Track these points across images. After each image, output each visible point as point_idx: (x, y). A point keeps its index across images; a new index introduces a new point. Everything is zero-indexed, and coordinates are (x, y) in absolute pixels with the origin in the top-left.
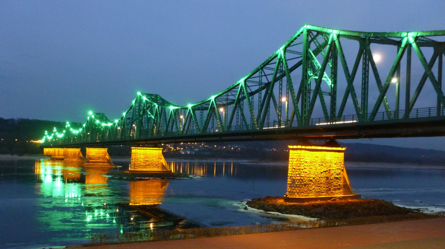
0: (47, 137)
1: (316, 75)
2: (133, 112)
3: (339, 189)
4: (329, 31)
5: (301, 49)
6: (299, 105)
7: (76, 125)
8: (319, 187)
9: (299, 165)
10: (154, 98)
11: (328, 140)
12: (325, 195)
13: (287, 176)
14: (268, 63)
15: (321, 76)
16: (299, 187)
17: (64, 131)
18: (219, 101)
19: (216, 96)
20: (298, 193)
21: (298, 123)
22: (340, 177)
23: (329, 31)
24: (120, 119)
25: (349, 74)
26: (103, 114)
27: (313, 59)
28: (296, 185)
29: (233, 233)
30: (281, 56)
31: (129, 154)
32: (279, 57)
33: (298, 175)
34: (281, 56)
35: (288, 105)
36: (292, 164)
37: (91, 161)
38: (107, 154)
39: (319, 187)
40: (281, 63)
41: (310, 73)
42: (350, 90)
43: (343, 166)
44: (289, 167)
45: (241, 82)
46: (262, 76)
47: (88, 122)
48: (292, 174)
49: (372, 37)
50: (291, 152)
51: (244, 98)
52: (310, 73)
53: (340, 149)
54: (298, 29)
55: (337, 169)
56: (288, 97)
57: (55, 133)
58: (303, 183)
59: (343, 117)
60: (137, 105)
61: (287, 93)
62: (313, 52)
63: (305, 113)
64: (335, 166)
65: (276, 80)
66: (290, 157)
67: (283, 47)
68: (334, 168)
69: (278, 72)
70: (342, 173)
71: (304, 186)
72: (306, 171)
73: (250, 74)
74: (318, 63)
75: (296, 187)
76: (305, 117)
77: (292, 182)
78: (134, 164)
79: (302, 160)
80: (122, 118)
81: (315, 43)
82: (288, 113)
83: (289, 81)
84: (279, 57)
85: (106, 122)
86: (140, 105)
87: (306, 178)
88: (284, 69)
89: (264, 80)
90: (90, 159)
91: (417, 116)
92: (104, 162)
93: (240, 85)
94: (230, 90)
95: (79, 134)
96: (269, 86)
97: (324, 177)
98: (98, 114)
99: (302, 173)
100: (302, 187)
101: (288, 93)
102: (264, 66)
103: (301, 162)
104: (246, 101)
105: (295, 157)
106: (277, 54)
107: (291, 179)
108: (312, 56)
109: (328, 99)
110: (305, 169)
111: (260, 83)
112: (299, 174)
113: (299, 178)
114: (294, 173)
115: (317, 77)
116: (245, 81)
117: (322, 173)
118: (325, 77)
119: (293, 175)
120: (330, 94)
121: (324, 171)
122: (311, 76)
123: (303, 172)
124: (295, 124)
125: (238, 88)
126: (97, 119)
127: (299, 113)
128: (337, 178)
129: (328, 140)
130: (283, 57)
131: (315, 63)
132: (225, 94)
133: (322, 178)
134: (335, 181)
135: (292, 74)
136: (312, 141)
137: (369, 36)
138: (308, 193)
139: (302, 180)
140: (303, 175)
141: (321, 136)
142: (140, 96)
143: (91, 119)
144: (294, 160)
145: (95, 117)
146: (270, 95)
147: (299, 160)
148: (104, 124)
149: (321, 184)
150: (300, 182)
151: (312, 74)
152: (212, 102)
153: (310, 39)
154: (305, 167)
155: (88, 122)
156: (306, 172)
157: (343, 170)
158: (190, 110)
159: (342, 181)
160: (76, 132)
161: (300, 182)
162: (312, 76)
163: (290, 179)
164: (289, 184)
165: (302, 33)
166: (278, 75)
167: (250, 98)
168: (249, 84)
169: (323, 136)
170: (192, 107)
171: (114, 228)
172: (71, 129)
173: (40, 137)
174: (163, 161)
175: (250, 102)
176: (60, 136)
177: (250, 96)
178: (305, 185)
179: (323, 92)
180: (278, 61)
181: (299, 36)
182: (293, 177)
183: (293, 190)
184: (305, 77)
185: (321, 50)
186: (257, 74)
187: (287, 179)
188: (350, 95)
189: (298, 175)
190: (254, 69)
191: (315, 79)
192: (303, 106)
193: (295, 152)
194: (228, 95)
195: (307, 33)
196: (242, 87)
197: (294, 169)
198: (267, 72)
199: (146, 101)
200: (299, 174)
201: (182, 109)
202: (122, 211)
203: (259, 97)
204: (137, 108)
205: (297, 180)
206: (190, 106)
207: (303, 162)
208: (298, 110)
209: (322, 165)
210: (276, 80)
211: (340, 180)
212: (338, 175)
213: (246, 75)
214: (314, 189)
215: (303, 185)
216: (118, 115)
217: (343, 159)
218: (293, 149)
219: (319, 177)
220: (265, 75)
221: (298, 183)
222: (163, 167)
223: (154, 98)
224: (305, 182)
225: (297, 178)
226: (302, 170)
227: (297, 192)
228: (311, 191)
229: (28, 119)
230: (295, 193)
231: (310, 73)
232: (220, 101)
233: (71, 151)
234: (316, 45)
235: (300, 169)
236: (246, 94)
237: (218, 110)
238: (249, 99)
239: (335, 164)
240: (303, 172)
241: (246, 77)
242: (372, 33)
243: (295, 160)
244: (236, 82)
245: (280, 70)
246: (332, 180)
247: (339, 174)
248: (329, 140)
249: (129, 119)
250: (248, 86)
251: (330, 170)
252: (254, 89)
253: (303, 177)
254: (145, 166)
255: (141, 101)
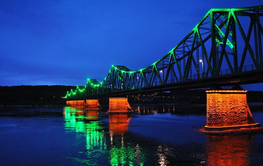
0: (68, 95)
1: (221, 41)
2: (110, 77)
3: (244, 120)
4: (228, 10)
5: (209, 26)
6: (212, 63)
7: (81, 87)
8: (230, 119)
9: (214, 104)
10: (120, 67)
11: (234, 86)
12: (235, 125)
13: (206, 112)
14: (187, 37)
15: (225, 42)
16: (215, 120)
17: (76, 91)
18: (159, 66)
19: (157, 62)
20: (215, 124)
21: (211, 74)
22: (245, 112)
23: (228, 10)
24: (103, 82)
25: (246, 37)
26: (95, 80)
27: (219, 31)
28: (213, 118)
29: (146, 112)
30: (196, 32)
31: (108, 102)
32: (195, 32)
33: (214, 111)
34: (196, 32)
35: (204, 64)
36: (209, 103)
37: (89, 107)
38: (98, 103)
39: (230, 119)
40: (197, 37)
41: (217, 40)
42: (248, 47)
43: (246, 103)
44: (207, 106)
45: (172, 52)
46: (184, 47)
47: (87, 84)
48: (209, 111)
49: (260, 9)
50: (208, 95)
51: (174, 63)
52: (217, 40)
53: (243, 91)
54: (206, 12)
55: (243, 106)
56: (203, 59)
57: (72, 93)
58: (218, 117)
59: (244, 67)
60: (112, 72)
61: (203, 57)
62: (219, 27)
63: (216, 68)
64: (240, 104)
65: (193, 49)
66: (208, 98)
67: (197, 25)
68: (240, 106)
69: (195, 43)
70: (246, 109)
71: (219, 119)
72: (220, 108)
73: (177, 46)
74: (222, 34)
75: (213, 120)
76: (216, 70)
77: (210, 116)
78: (111, 108)
79: (216, 100)
80: (104, 81)
81: (219, 20)
82: (204, 69)
83: (204, 48)
84: (195, 32)
85: (94, 84)
86: (113, 73)
87: (220, 113)
88: (199, 41)
89: (187, 49)
90: (89, 106)
91: (245, 70)
92: (96, 108)
93: (171, 54)
94: (165, 58)
95: (83, 92)
96: (190, 53)
97: (233, 112)
98: (92, 80)
99: (217, 110)
100: (218, 120)
101: (203, 56)
102: (185, 40)
103: (216, 101)
104: (175, 65)
105: (211, 98)
106: (193, 30)
107: (209, 114)
108: (217, 29)
109: (231, 58)
110: (219, 106)
111: (184, 52)
112: (215, 110)
113: (215, 113)
114: (211, 110)
115: (222, 43)
116: (174, 51)
117: (231, 109)
118: (228, 43)
119: (210, 111)
120: (232, 54)
121: (233, 108)
122: (218, 42)
123: (218, 109)
124: (210, 75)
125: (170, 56)
126: (92, 83)
127: (211, 68)
128: (243, 113)
129: (234, 86)
130: (198, 32)
131: (220, 34)
132: (162, 61)
133: (232, 112)
134: (241, 115)
135: (205, 44)
136: (223, 87)
137: (258, 8)
138: (222, 124)
139: (217, 115)
140: (218, 111)
141: (228, 83)
142: (114, 67)
143: (89, 83)
144: (210, 100)
145: (91, 82)
146: (191, 58)
147: (214, 100)
148: (95, 86)
149: (231, 117)
150: (215, 116)
151: (218, 41)
152: (172, 55)
153: (215, 18)
154: (219, 105)
155: (87, 84)
156: (220, 109)
157: (246, 107)
158: (141, 73)
159: (247, 114)
160: (81, 91)
161: (215, 116)
162: (219, 42)
163: (208, 114)
164: (208, 118)
165: (209, 14)
166: (195, 46)
167: (179, 62)
168: (177, 53)
169: (231, 82)
170: (143, 71)
171: (105, 145)
172: (79, 90)
173: (65, 96)
174: (128, 106)
175: (178, 65)
176: (74, 94)
177: (178, 61)
178: (220, 118)
179: (228, 52)
180: (194, 35)
181: (207, 17)
182: (211, 113)
183: (211, 122)
184: (214, 43)
185: (224, 25)
186: (181, 46)
187: (207, 114)
188: (248, 51)
189: (214, 111)
190: (179, 42)
191: (221, 44)
192: (214, 63)
193: (211, 95)
194: (163, 61)
195: (212, 14)
196: (172, 55)
197: (211, 107)
198: (188, 44)
199: (117, 70)
200: (215, 110)
201: (137, 72)
202: (101, 152)
203: (197, 53)
204: (112, 74)
205: (213, 115)
206: (141, 70)
207: (217, 102)
208: (211, 66)
209: (231, 103)
210: (193, 49)
211: (245, 114)
212: (243, 110)
213: (174, 47)
214: (226, 121)
215: (218, 118)
216: (102, 79)
217: (246, 98)
218: (209, 93)
219: (230, 112)
220: (187, 46)
221: (214, 117)
222: (128, 109)
223: (120, 67)
224: (219, 116)
225: (213, 113)
226: (217, 107)
227: (214, 123)
228: (224, 122)
229: (7, 86)
230: (212, 124)
231: (217, 40)
232: (160, 66)
233: (79, 101)
234: (220, 22)
235: (215, 107)
236: (175, 61)
237: (158, 73)
238: (178, 64)
239: (241, 102)
240: (218, 109)
241: (174, 48)
242: (260, 6)
243: (211, 100)
244: (168, 52)
245: (196, 41)
246: (239, 114)
247: (244, 109)
248: (234, 86)
249: (108, 81)
250: (176, 55)
251: (237, 107)
252: (181, 56)
253: (217, 112)
254: (118, 109)
255: (114, 70)
